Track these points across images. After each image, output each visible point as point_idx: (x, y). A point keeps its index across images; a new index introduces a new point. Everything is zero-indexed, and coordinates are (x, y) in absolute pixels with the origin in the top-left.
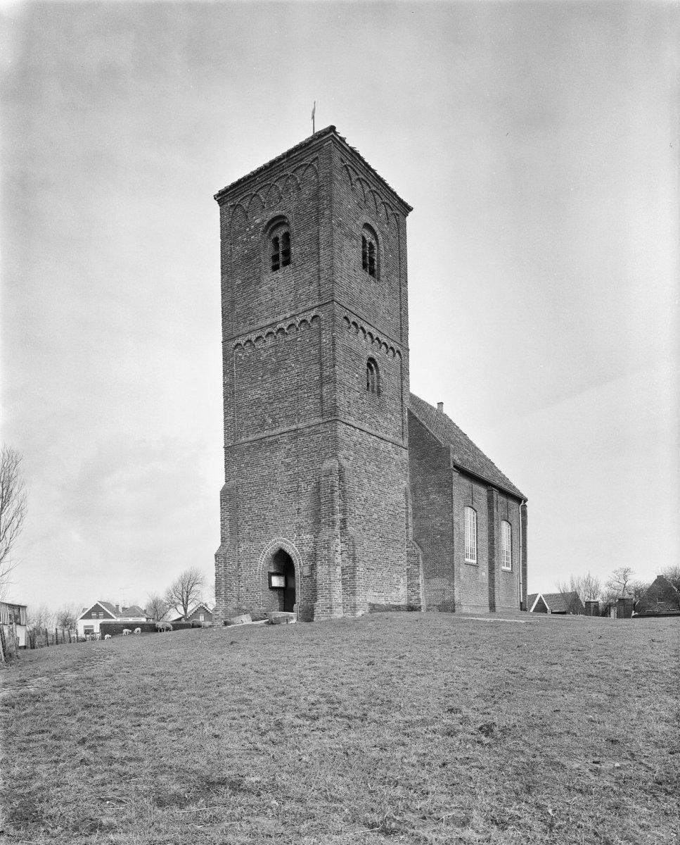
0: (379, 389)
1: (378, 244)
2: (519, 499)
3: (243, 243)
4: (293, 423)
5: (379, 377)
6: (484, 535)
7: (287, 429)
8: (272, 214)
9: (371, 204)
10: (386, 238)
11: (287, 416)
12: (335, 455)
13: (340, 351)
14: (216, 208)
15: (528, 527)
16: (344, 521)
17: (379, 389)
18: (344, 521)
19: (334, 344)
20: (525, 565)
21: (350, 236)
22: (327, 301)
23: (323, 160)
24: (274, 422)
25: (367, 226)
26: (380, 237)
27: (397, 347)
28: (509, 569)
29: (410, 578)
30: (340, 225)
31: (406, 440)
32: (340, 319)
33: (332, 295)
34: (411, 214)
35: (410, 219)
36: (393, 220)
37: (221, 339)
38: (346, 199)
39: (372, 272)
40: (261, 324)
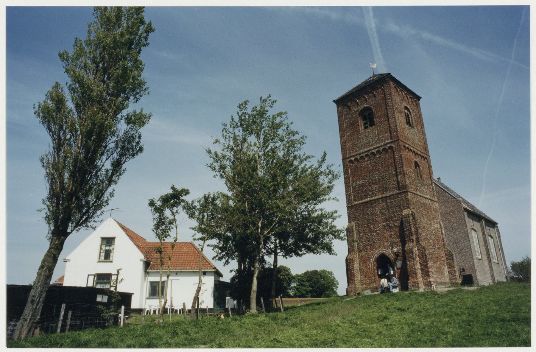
0: (421, 175)
1: (410, 113)
2: (492, 224)
3: (349, 118)
4: (383, 193)
5: (420, 170)
6: (482, 243)
7: (380, 196)
8: (362, 107)
9: (406, 98)
10: (413, 111)
11: (379, 191)
12: (408, 207)
13: (404, 160)
14: (335, 105)
15: (501, 238)
16: (418, 239)
17: (421, 175)
18: (418, 239)
19: (401, 157)
20: (504, 259)
21: (400, 112)
22: (396, 139)
23: (381, 83)
24: (373, 193)
25: (406, 108)
26: (411, 111)
27: (425, 156)
28: (496, 261)
29: (449, 268)
30: (397, 109)
31: (436, 198)
32: (402, 147)
33: (398, 137)
34: (421, 100)
35: (421, 102)
36: (414, 103)
37: (341, 158)
38: (398, 100)
39: (410, 125)
40: (362, 151)
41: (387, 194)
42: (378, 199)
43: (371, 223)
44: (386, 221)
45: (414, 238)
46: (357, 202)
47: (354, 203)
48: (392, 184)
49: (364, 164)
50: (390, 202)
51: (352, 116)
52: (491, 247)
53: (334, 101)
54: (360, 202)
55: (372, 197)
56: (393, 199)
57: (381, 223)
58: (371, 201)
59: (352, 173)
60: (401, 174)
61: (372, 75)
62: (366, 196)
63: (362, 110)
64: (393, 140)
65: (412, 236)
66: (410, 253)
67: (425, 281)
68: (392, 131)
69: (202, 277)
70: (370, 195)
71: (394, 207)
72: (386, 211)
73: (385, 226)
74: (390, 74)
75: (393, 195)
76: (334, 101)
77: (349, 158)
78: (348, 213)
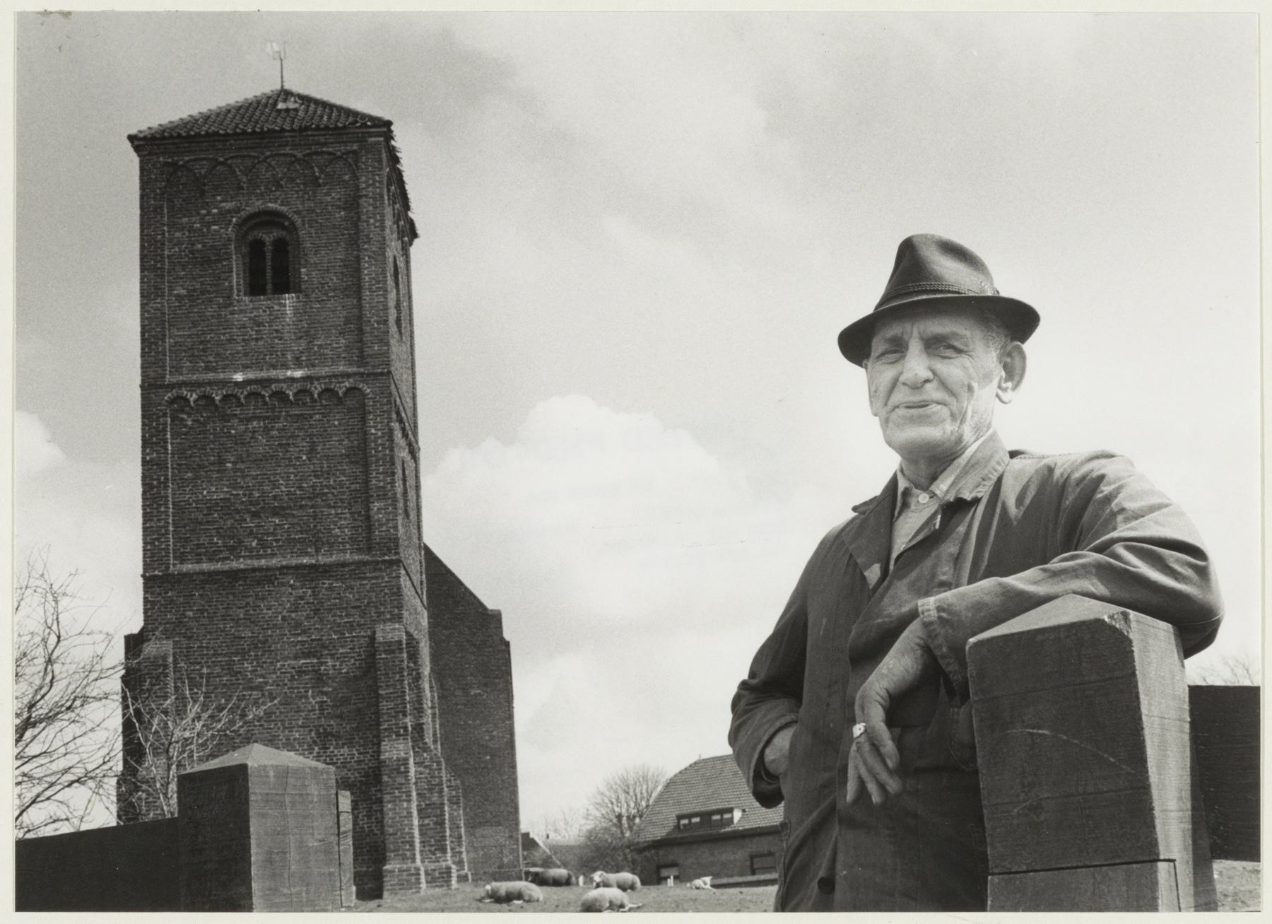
11: (289, 541)
24: (263, 545)
35: (416, 241)
41: (322, 560)
42: (284, 569)
43: (244, 654)
44: (306, 655)
45: (409, 721)
46: (188, 567)
47: (176, 568)
48: (342, 527)
49: (236, 428)
50: (331, 588)
51: (208, 225)
52: (1173, 804)
53: (132, 138)
54: (205, 566)
55: (259, 557)
56: (343, 580)
57: (286, 659)
58: (254, 570)
59: (180, 452)
60: (379, 498)
61: (279, 87)
62: (234, 551)
63: (251, 216)
64: (369, 369)
65: (405, 715)
66: (399, 772)
67: (432, 866)
68: (367, 338)
69: (1162, 857)
70: (251, 550)
71: (341, 609)
72: (308, 618)
73: (301, 672)
74: (384, 128)
75: (344, 565)
76: (132, 138)
77: (172, 386)
78: (146, 601)
